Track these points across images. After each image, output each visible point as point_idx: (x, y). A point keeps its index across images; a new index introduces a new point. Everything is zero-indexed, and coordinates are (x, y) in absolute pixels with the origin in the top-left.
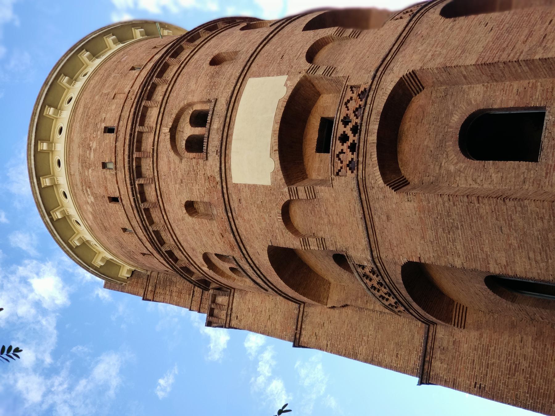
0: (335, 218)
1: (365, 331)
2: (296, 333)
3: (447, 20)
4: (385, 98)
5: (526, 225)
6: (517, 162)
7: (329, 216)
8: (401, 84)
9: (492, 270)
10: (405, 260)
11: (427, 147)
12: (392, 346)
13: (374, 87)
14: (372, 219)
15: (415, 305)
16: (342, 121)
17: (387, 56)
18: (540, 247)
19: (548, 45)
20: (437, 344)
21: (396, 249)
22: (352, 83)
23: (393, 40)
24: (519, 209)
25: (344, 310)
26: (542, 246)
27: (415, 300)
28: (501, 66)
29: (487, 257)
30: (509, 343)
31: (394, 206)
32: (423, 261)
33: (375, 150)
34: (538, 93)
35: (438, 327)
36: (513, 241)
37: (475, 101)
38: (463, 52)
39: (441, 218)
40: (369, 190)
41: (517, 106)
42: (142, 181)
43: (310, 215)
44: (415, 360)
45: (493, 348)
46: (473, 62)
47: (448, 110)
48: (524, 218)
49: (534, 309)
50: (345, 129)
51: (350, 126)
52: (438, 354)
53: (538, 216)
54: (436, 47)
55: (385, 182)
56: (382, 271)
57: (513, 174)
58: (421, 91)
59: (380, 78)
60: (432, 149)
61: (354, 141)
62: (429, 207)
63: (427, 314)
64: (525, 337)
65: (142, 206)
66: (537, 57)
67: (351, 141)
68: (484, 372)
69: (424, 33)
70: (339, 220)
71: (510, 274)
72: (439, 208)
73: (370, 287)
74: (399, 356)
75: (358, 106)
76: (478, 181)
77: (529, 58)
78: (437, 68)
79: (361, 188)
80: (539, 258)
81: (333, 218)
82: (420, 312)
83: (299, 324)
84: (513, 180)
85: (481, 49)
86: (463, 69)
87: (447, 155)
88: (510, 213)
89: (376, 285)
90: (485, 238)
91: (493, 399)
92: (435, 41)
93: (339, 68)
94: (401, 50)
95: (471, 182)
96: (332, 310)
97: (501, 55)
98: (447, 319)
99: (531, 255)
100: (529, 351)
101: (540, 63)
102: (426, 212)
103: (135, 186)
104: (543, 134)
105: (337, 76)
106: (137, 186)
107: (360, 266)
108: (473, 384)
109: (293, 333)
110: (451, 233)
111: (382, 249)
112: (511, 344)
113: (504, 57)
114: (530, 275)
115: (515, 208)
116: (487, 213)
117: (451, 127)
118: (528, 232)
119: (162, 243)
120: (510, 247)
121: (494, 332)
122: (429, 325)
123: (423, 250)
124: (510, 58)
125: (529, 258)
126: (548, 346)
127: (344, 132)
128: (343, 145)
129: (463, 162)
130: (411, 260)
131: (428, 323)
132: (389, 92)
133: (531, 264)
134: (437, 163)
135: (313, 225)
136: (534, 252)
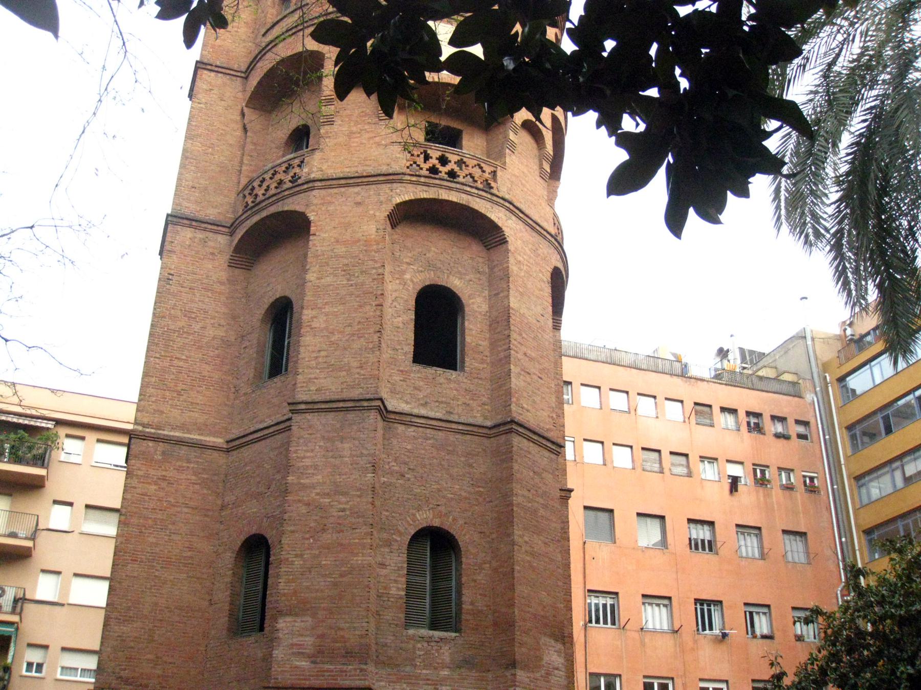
0: (356, 140)
1: (218, 150)
3: (549, 275)
4: (483, 211)
5: (353, 351)
6: (413, 343)
7: (359, 133)
9: (305, 312)
10: (312, 218)
11: (429, 251)
12: (202, 181)
13: (495, 198)
14: (357, 185)
15: (256, 218)
16: (462, 160)
17: (523, 213)
18: (332, 363)
19: (522, 377)
20: (211, 235)
23: (535, 218)
24: (371, 346)
25: (240, 126)
27: (263, 219)
28: (506, 332)
29: (319, 308)
31: (371, 212)
32: (311, 238)
33: (431, 197)
34: (476, 365)
35: (228, 237)
36: (337, 336)
37: (473, 303)
38: (522, 294)
39: (359, 263)
40: (389, 185)
41: (466, 344)
43: (360, 110)
44: (190, 209)
45: (210, 295)
46: (512, 305)
47: (465, 274)
48: (360, 349)
49: (255, 342)
50: (453, 162)
51: (456, 169)
52: (200, 235)
53: (364, 363)
54: (527, 265)
55: (397, 205)
56: (298, 189)
57: (402, 339)
58: (485, 246)
59: (503, 206)
61: (441, 172)
62: (371, 251)
63: (244, 230)
64: (225, 329)
66: (512, 367)
67: (441, 168)
68: (185, 285)
69: (540, 251)
70: (355, 145)
71: (302, 331)
72: (370, 263)
74: (193, 189)
75: (476, 178)
76: (395, 304)
77: (512, 359)
78: (508, 267)
79: (391, 177)
80: (320, 360)
81: (356, 138)
82: (248, 222)
83: (223, 70)
84: (396, 339)
85: (522, 312)
86: (505, 293)
87: (422, 272)
88: (366, 336)
89: (277, 177)
90: (339, 308)
91: (158, 292)
92: (532, 264)
93: (514, 157)
94: (527, 227)
95: (394, 296)
96: (239, 111)
97: (515, 332)
98: (238, 249)
99: (323, 353)
100: (211, 333)
104: (439, 369)
105: (507, 155)
107: (302, 162)
108: (172, 272)
109: (211, 62)
110: (343, 273)
111: (323, 192)
113: (514, 335)
114: (302, 350)
115: (372, 342)
116: (366, 313)
117: (448, 277)
118: (347, 352)
120: (331, 333)
121: (227, 298)
122: (229, 228)
123: (324, 239)
124: (513, 341)
125: (320, 351)
127: (450, 161)
128: (437, 159)
129: (414, 288)
130: (312, 224)
131: (232, 229)
132: (489, 215)
133: (313, 352)
134: (412, 260)
135: (348, 112)
136: (326, 356)
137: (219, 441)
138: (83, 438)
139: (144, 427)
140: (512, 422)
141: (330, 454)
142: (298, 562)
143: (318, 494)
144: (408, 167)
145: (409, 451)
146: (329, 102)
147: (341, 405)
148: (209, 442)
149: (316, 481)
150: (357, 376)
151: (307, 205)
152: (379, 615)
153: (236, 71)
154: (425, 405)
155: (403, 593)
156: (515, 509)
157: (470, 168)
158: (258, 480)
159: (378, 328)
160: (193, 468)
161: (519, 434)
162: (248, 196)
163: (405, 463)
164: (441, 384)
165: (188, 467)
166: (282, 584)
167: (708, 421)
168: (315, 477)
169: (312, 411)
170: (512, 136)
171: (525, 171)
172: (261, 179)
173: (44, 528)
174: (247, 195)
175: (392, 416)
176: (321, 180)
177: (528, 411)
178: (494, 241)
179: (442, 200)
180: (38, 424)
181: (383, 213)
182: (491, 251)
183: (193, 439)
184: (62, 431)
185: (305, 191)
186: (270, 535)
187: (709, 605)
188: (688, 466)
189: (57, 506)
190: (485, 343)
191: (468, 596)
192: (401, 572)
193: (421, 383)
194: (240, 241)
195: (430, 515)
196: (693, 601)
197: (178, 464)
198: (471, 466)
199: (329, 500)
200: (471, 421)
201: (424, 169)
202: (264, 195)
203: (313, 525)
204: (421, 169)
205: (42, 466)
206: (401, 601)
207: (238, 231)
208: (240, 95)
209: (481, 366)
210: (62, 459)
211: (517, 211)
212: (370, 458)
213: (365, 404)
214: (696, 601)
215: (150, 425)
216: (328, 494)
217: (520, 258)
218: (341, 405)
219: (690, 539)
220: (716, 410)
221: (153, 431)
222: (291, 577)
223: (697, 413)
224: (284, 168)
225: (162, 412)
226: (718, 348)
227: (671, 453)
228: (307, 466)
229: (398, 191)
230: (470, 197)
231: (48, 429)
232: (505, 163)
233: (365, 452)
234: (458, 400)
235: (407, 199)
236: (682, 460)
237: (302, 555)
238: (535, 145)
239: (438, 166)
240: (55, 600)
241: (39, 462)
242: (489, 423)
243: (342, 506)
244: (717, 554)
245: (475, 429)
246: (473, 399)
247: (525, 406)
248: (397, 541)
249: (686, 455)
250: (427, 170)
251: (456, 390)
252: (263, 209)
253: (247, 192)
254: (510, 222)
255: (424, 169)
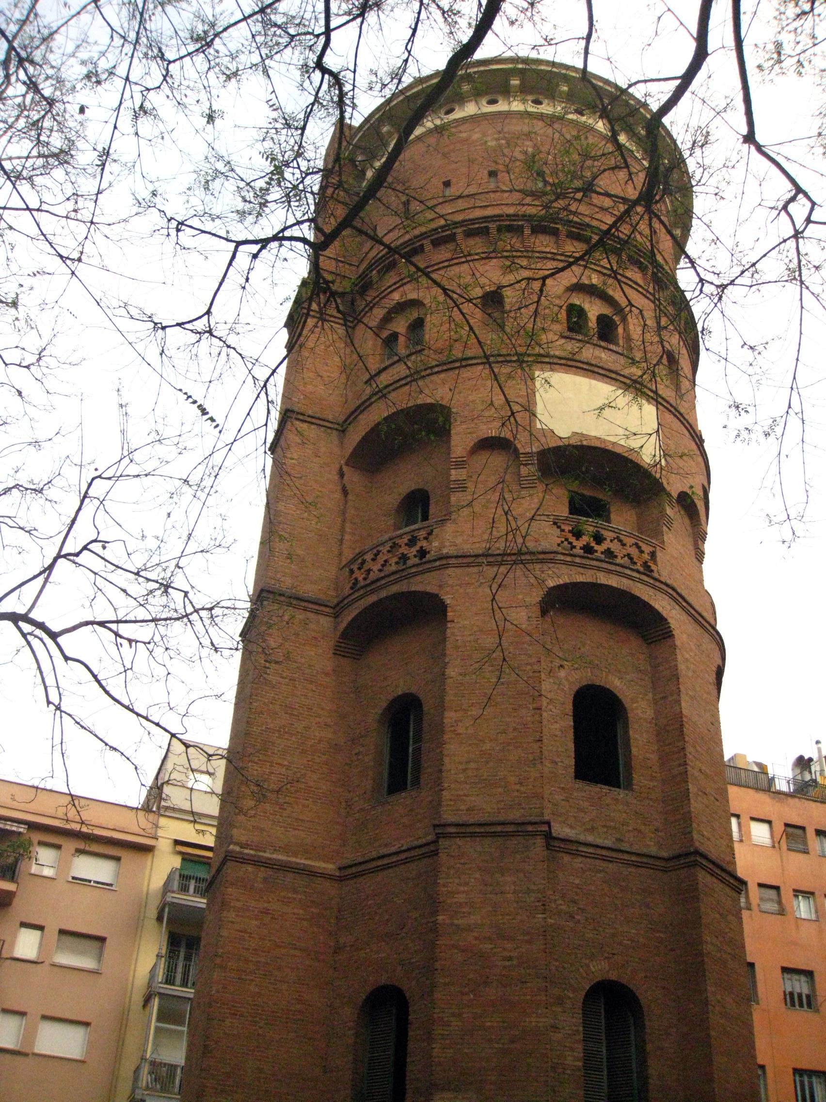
2: (304, 415)
4: (645, 598)
5: (510, 763)
6: (573, 755)
8: (659, 620)
9: (447, 714)
11: (584, 645)
13: (657, 584)
15: (372, 599)
21: (461, 591)
22: (659, 554)
24: (531, 757)
26: (485, 780)
28: (680, 744)
29: (464, 710)
30: (323, 709)
32: (449, 625)
33: (589, 580)
35: (332, 619)
37: (637, 708)
42: (527, 231)
45: (314, 689)
46: (684, 712)
52: (300, 616)
57: (560, 749)
60: (582, 649)
61: (596, 551)
63: (357, 611)
65: (493, 226)
66: (690, 786)
67: (596, 547)
68: (285, 675)
73: (397, 541)
75: (635, 560)
76: (551, 707)
80: (470, 773)
86: (675, 697)
88: (525, 746)
101: (682, 789)
102: (516, 639)
103: (521, 220)
106: (520, 223)
110: (491, 668)
111: (459, 571)
112: (321, 712)
113: (689, 749)
116: (522, 717)
119: (436, 243)
122: (334, 608)
126: (324, 758)
129: (570, 689)
130: (449, 609)
131: (337, 610)
132: (652, 603)
137: (330, 867)
138: (58, 847)
139: (241, 847)
140: (697, 852)
141: (490, 889)
142: (455, 1022)
143: (476, 938)
144: (559, 545)
145: (577, 886)
146: (460, 464)
147: (499, 829)
148: (319, 867)
149: (473, 922)
150: (516, 794)
151: (440, 586)
152: (554, 1092)
153: (332, 423)
154: (592, 830)
155: (580, 1064)
156: (706, 959)
157: (627, 547)
158: (387, 917)
159: (538, 735)
160: (300, 900)
161: (704, 868)
162: (357, 572)
163: (574, 902)
164: (608, 805)
165: (295, 899)
166: (436, 1050)
167: (801, 847)
168: (472, 917)
169: (462, 835)
170: (669, 511)
171: (682, 551)
172: (375, 551)
173: (8, 956)
174: (355, 569)
175: (556, 843)
176: (457, 557)
177: (709, 839)
178: (657, 634)
179: (601, 585)
180: (8, 827)
181: (536, 596)
182: (653, 646)
183: (298, 864)
184: (36, 837)
185: (438, 568)
186: (409, 987)
187: (810, 1077)
188: (780, 902)
189: (23, 930)
190: (654, 757)
191: (654, 1068)
192: (577, 1038)
193: (586, 804)
194: (350, 624)
195: (605, 965)
196: (791, 1071)
197: (282, 894)
198: (647, 906)
199: (490, 946)
200: (645, 851)
201: (578, 548)
202: (380, 571)
203: (471, 976)
204: (575, 547)
205: (12, 879)
206: (578, 1073)
207: (346, 612)
208: (336, 450)
209: (651, 784)
210: (33, 871)
211: (680, 600)
212: (540, 895)
213: (530, 828)
214: (795, 1071)
215: (248, 845)
216: (490, 939)
217: (687, 656)
218: (499, 829)
219: (784, 992)
220: (810, 833)
221: (252, 852)
222: (448, 1042)
223: (788, 836)
224: (406, 540)
225: (262, 830)
226: (797, 755)
227: (760, 885)
228: (460, 903)
229: (550, 572)
230: (631, 582)
231: (20, 833)
232: (663, 542)
233: (532, 887)
234: (628, 824)
235: (562, 582)
236: (772, 893)
237: (460, 1015)
238: (687, 521)
239: (593, 544)
240: (17, 1048)
241: (8, 874)
242: (664, 854)
243: (506, 954)
244: (817, 1011)
245: (651, 861)
246: (645, 825)
247: (705, 833)
248: (569, 998)
249: (777, 888)
250: (581, 548)
251: (625, 812)
252: (381, 588)
253: (355, 567)
254: (674, 611)
255: (578, 548)
